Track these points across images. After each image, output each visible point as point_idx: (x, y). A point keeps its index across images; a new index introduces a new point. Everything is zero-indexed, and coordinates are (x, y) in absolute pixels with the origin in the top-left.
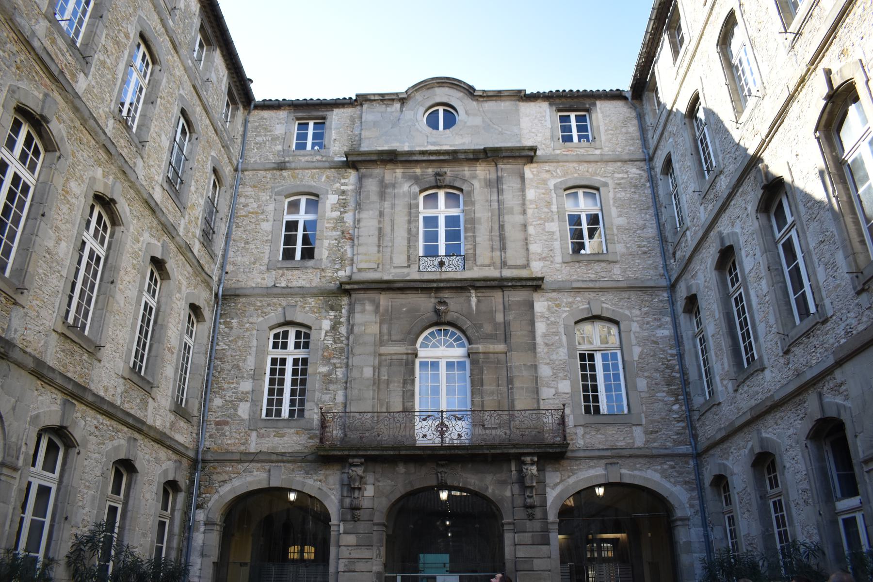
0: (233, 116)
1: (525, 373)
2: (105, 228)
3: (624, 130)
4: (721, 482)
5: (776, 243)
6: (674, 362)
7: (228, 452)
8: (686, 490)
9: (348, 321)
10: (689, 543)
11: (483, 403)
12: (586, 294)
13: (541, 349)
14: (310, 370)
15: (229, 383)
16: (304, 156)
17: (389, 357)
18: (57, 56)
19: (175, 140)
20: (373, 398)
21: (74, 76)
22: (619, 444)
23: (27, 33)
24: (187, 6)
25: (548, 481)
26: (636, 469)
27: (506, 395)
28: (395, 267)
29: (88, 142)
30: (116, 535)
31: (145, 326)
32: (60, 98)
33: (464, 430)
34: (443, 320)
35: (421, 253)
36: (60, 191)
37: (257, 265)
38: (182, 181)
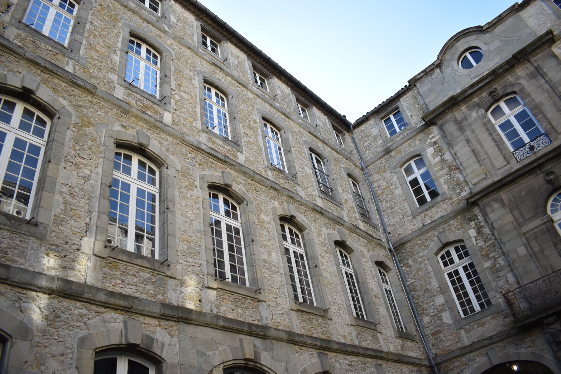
0: (344, 139)
2: (297, 236)
7: (450, 352)
9: (486, 221)
14: (478, 269)
15: (427, 303)
16: (398, 137)
17: (531, 233)
18: (220, 150)
20: (537, 268)
21: (235, 156)
23: (196, 143)
24: (283, 92)
28: (498, 169)
31: (352, 287)
32: (232, 171)
35: (512, 150)
36: (257, 223)
37: (406, 218)
38: (331, 189)
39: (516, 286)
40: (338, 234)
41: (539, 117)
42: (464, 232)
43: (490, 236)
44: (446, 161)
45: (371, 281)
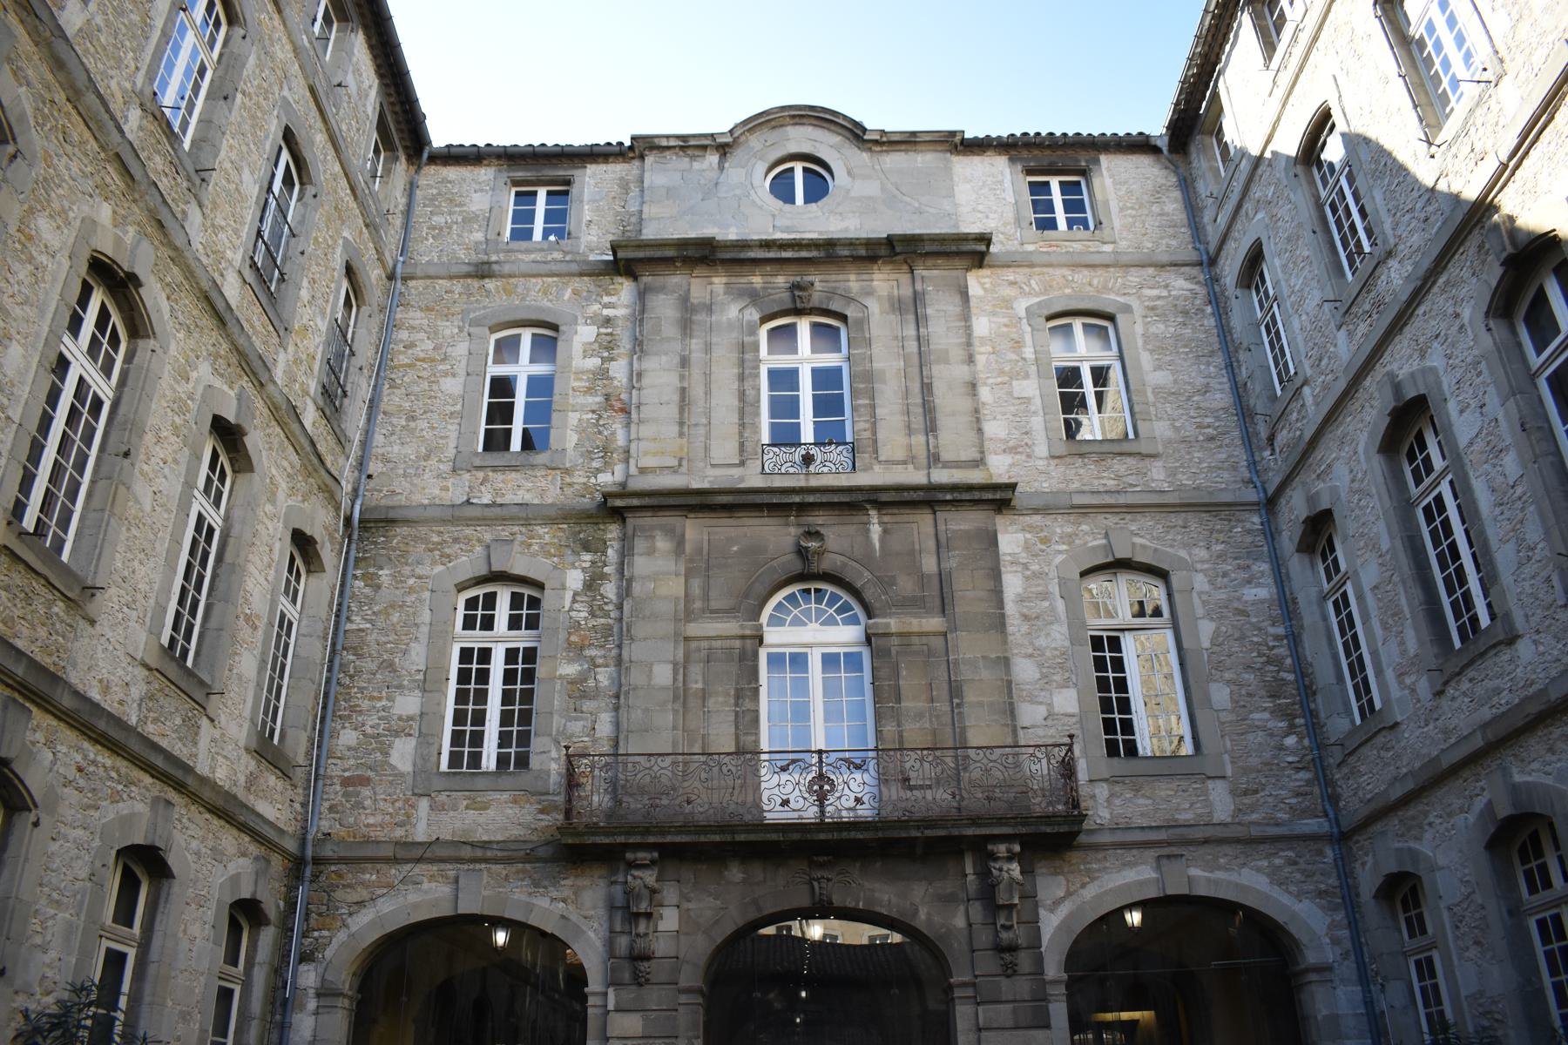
0: (388, 171)
1: (985, 674)
2: (115, 341)
3: (1155, 208)
4: (1403, 890)
5: (1533, 376)
6: (1283, 651)
7: (367, 841)
8: (1322, 908)
9: (621, 571)
10: (1334, 1018)
11: (901, 736)
12: (1100, 517)
13: (1015, 625)
14: (541, 670)
15: (372, 698)
16: (528, 251)
17: (705, 644)
19: (270, 189)
20: (675, 728)
22: (1185, 817)
25: (1041, 895)
26: (1219, 868)
27: (947, 719)
29: (83, 143)
30: (121, 1016)
31: (197, 564)
33: (867, 789)
34: (814, 568)
35: (766, 439)
36: (12, 230)
37: (433, 462)
38: (281, 274)
39: (606, 749)
40: (235, 402)
41: (860, 402)
42: (555, 568)
43: (610, 607)
44: (608, 378)
45: (256, 573)
